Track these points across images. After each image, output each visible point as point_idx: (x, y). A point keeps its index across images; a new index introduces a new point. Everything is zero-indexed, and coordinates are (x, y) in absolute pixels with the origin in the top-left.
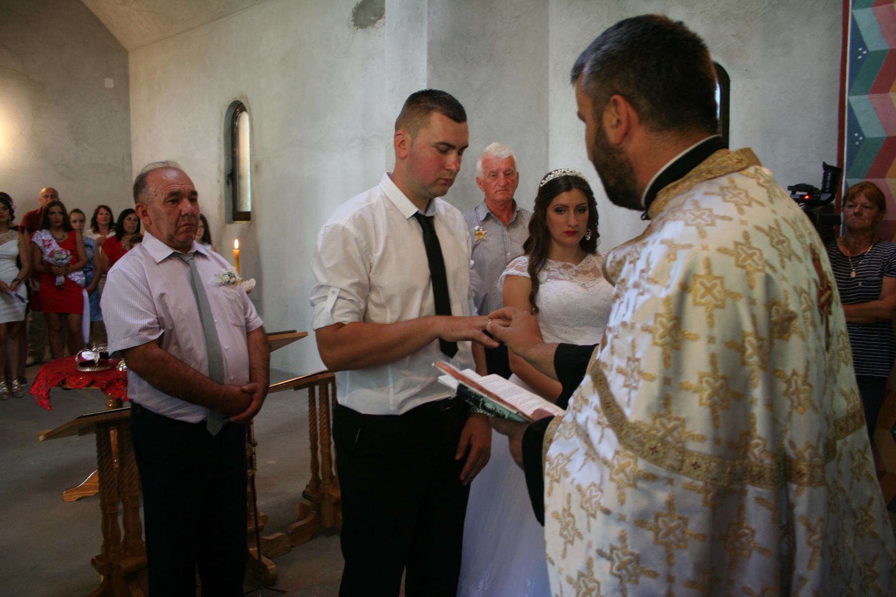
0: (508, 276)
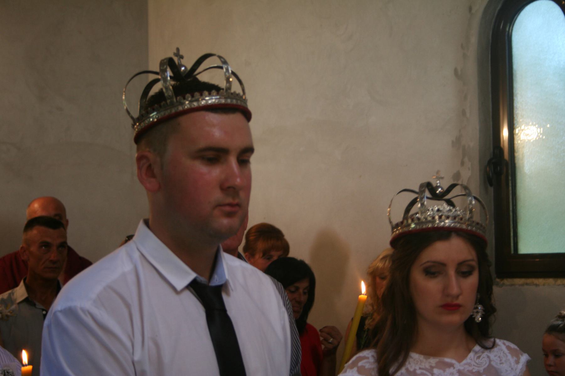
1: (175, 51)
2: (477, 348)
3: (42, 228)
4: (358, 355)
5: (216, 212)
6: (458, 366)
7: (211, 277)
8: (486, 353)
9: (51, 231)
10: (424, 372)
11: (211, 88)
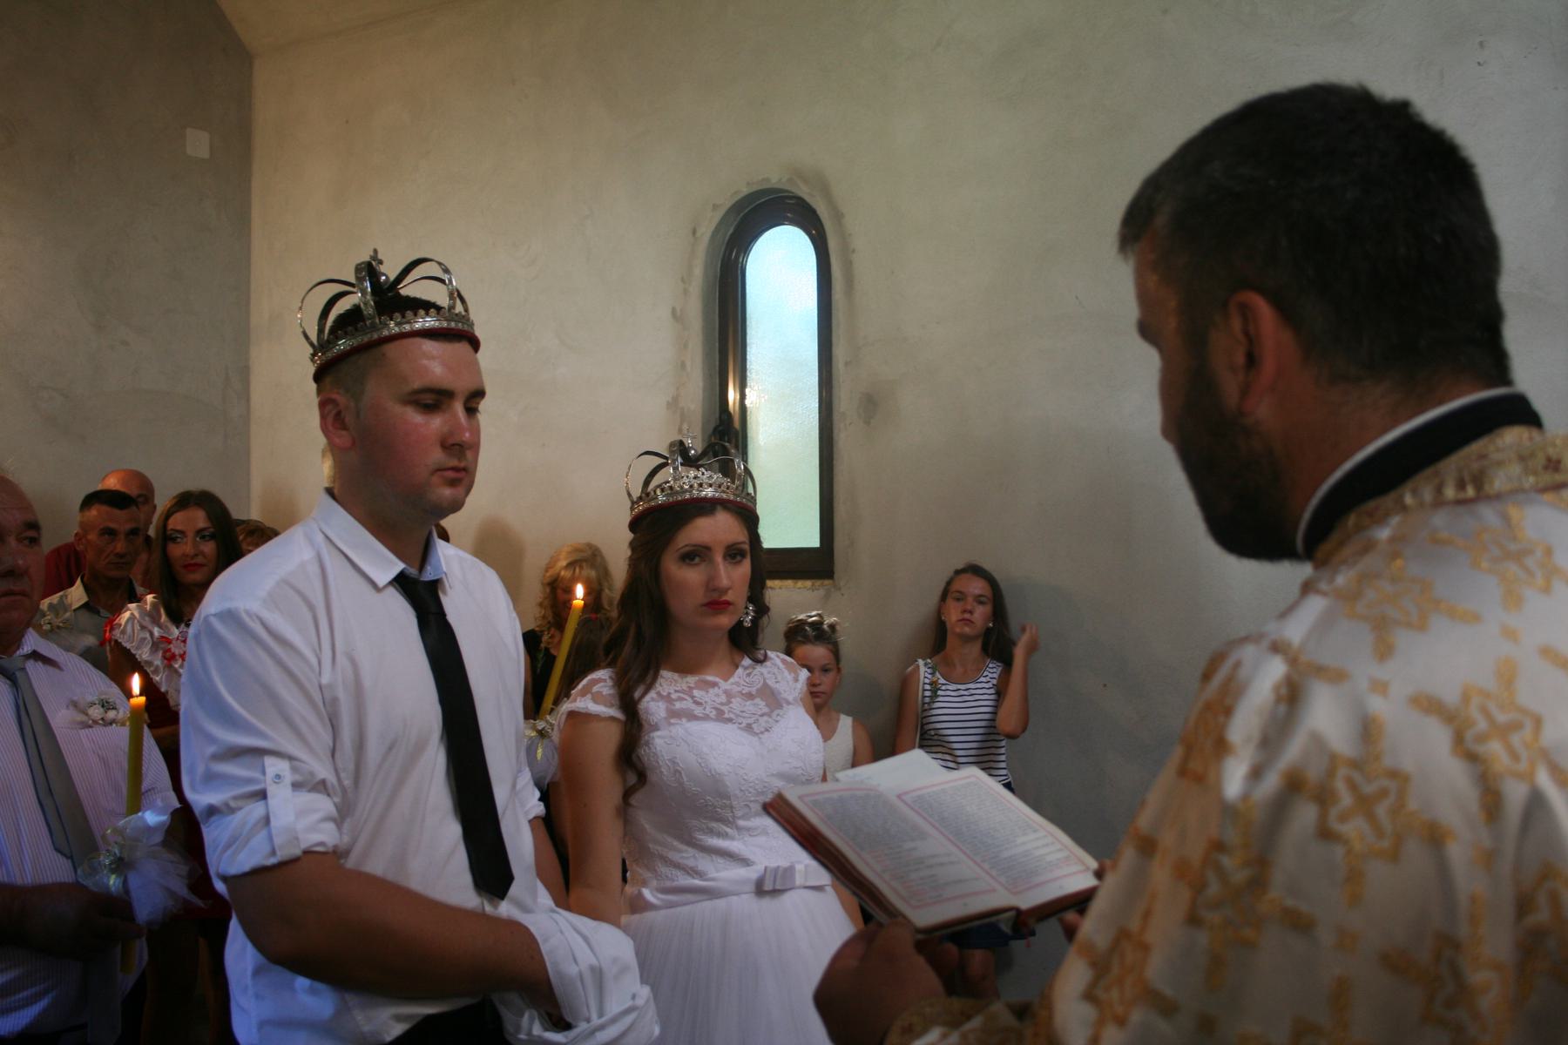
0: (572, 715)
1: (372, 254)
2: (747, 661)
3: (105, 508)
4: (589, 677)
5: (435, 479)
6: (724, 685)
7: (421, 568)
8: (759, 668)
9: (117, 512)
10: (682, 695)
11: (427, 306)
